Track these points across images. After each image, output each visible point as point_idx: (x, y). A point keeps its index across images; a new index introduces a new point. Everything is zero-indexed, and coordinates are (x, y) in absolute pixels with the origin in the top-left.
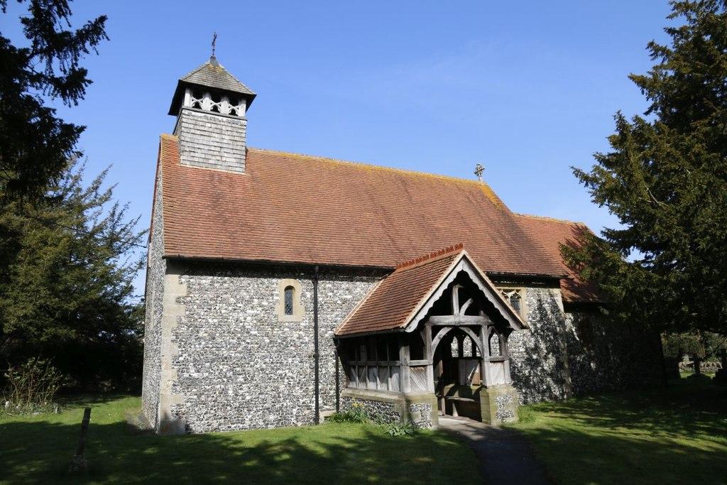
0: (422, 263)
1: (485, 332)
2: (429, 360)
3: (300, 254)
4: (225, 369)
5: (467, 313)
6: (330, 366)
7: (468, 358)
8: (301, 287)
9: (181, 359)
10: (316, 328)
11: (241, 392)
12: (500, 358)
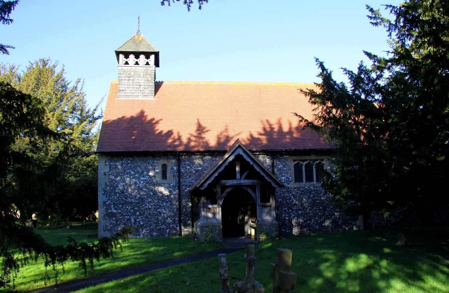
5: (245, 179)
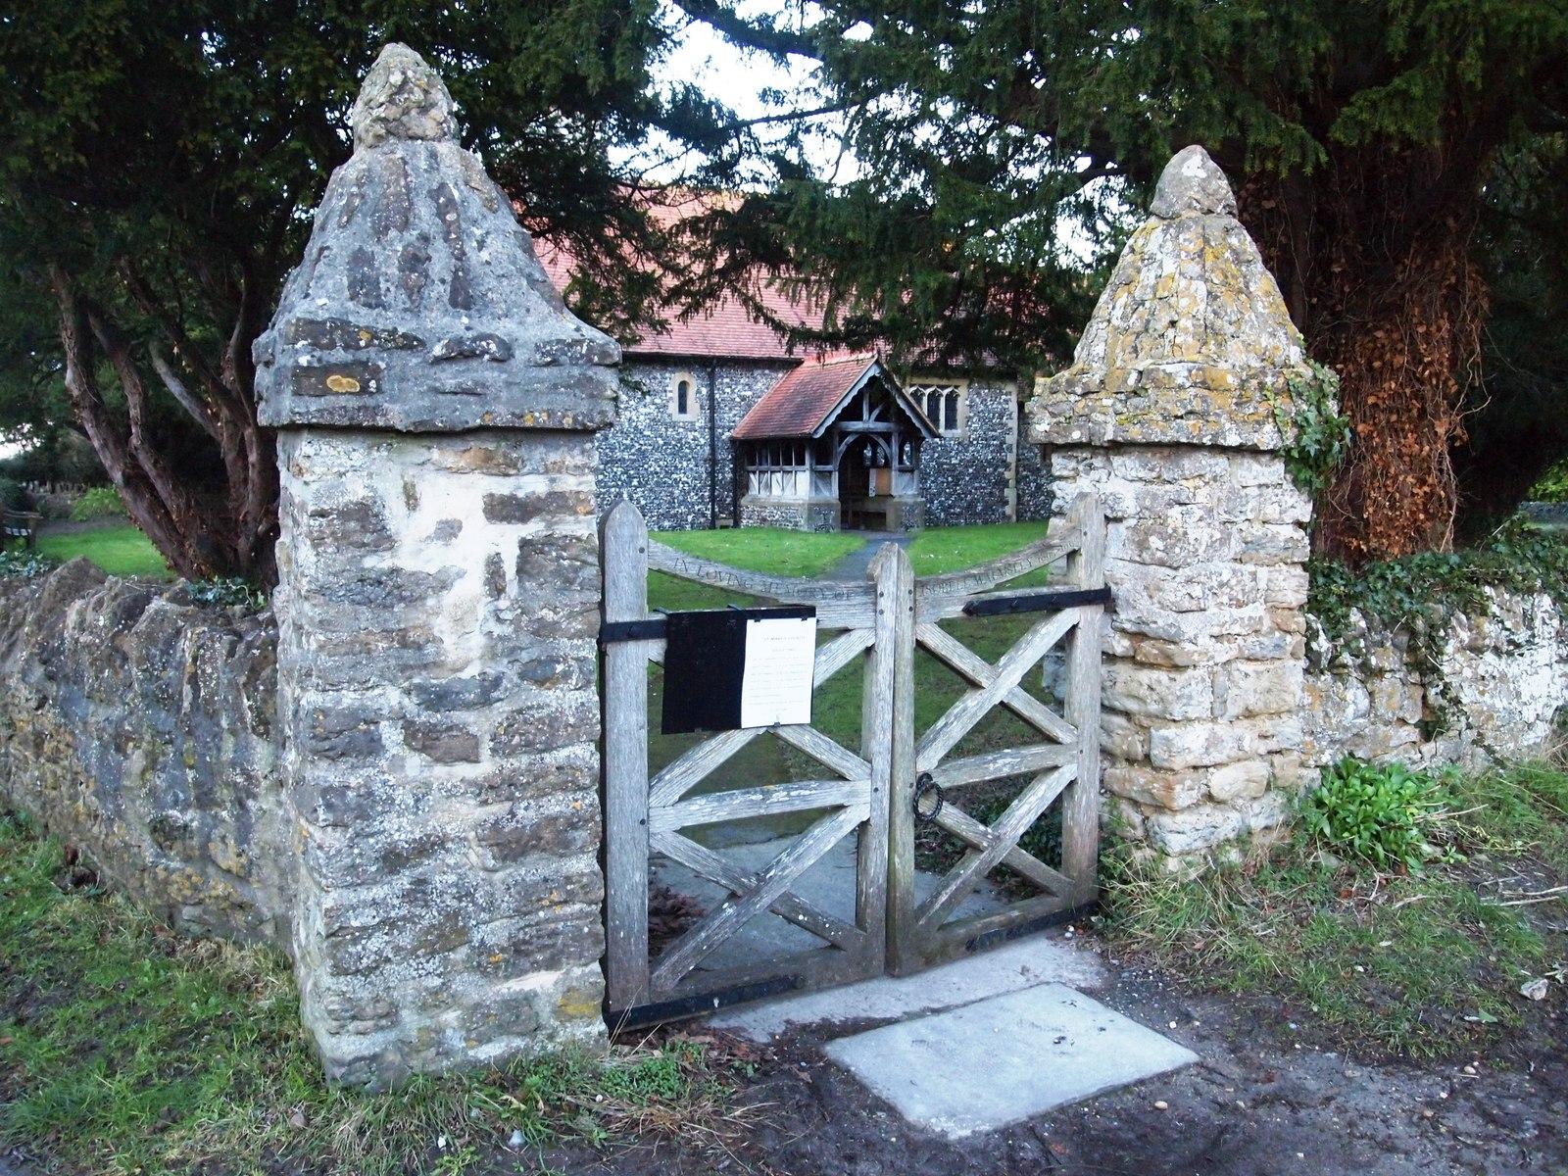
5: (878, 419)
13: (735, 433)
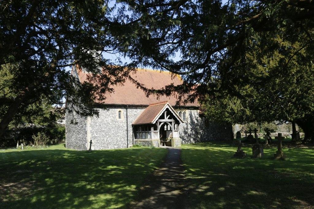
0: (157, 105)
1: (173, 124)
2: (158, 130)
3: (122, 101)
4: (104, 133)
5: (168, 119)
6: (131, 133)
7: (169, 130)
8: (123, 111)
9: (92, 131)
10: (127, 122)
11: (108, 140)
12: (177, 130)
13: (133, 123)
